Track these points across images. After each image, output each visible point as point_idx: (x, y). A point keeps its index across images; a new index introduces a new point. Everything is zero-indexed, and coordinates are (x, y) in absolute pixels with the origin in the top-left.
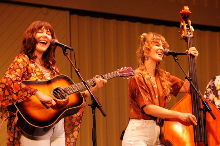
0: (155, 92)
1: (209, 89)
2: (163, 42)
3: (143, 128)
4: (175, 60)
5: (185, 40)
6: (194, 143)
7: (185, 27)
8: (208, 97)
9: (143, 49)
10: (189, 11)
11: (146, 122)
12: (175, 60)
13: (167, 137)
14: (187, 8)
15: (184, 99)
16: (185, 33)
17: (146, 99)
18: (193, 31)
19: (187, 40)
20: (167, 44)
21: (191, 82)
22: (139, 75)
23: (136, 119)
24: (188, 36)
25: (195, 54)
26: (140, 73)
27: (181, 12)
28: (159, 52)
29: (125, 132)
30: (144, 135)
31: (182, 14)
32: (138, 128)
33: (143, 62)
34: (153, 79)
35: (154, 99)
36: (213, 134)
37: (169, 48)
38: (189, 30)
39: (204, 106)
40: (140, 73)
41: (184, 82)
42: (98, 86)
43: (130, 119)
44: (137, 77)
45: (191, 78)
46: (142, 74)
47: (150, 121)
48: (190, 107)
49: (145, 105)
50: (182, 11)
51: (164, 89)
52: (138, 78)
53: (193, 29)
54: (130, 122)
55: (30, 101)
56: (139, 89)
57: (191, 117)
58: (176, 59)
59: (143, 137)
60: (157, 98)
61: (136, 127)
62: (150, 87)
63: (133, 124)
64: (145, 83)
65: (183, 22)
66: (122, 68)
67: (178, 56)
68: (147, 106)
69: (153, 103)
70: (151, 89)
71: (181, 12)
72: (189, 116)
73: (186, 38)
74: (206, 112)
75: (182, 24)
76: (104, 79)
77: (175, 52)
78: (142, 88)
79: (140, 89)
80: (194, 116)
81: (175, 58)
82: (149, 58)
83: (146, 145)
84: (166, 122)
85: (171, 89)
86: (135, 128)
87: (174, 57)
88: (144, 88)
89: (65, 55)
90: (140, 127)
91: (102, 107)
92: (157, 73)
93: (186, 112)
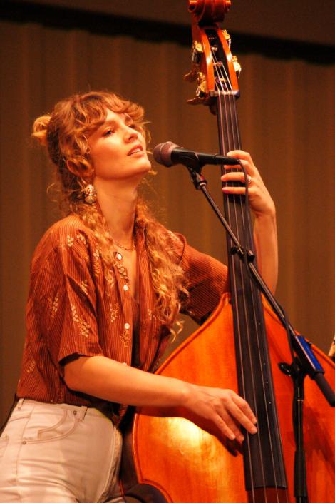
0: (124, 310)
3: (65, 435)
4: (196, 184)
5: (208, 107)
11: (75, 413)
12: (196, 184)
13: (148, 473)
16: (207, 79)
17: (85, 333)
18: (237, 73)
22: (76, 239)
26: (83, 233)
32: (44, 435)
35: (113, 332)
38: (223, 69)
40: (83, 233)
43: (17, 399)
44: (67, 247)
45: (251, 253)
46: (86, 238)
47: (90, 410)
48: (227, 365)
49: (75, 356)
52: (71, 248)
53: (237, 67)
54: (16, 409)
57: (233, 406)
58: (199, 178)
64: (92, 273)
65: (200, 41)
67: (206, 169)
68: (81, 358)
69: (103, 346)
72: (223, 400)
73: (211, 102)
75: (199, 47)
78: (77, 289)
79: (71, 295)
80: (243, 401)
81: (194, 177)
83: (72, 498)
84: (139, 419)
86: (33, 434)
87: (191, 172)
88: (84, 289)
89: (197, 188)
93: (214, 385)
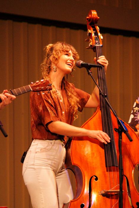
1: (137, 108)
2: (73, 52)
3: (49, 150)
4: (89, 73)
5: (92, 50)
6: (106, 168)
7: (93, 35)
8: (135, 117)
9: (51, 59)
10: (97, 16)
11: (51, 143)
12: (89, 73)
14: (94, 13)
15: (93, 117)
16: (92, 41)
18: (102, 39)
19: (95, 50)
20: (77, 55)
21: (106, 98)
23: (40, 139)
24: (96, 45)
25: (105, 64)
27: (87, 17)
28: (69, 63)
29: (26, 154)
30: (48, 158)
31: (89, 20)
32: (42, 150)
33: (49, 73)
34: (59, 93)
36: (130, 156)
37: (81, 59)
38: (97, 38)
39: (119, 126)
41: (89, 95)
42: (4, 103)
45: (106, 95)
50: (89, 16)
51: (71, 105)
53: (102, 37)
54: (33, 142)
55: (103, 192)
56: (44, 103)
58: (90, 72)
59: (46, 160)
60: (64, 114)
61: (107, 173)
62: (56, 101)
63: (37, 145)
64: (52, 97)
65: (90, 29)
66: (38, 81)
67: (92, 69)
70: (57, 103)
71: (87, 17)
73: (94, 48)
74: (122, 132)
75: (90, 31)
76: (13, 95)
77: (89, 64)
78: (48, 102)
79: (46, 104)
81: (88, 71)
82: (57, 70)
84: (74, 143)
85: (80, 106)
86: (39, 150)
87: (87, 70)
88: (50, 102)
90: (45, 148)
91: (2, 127)
92: (63, 85)
